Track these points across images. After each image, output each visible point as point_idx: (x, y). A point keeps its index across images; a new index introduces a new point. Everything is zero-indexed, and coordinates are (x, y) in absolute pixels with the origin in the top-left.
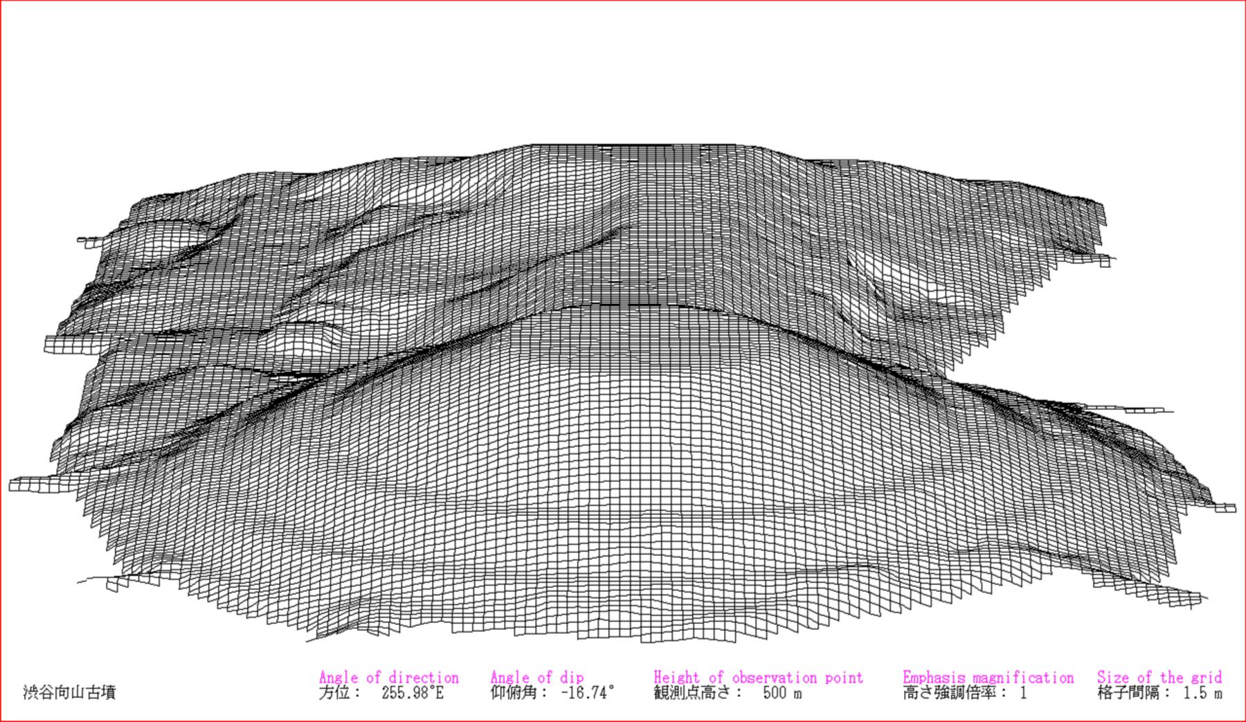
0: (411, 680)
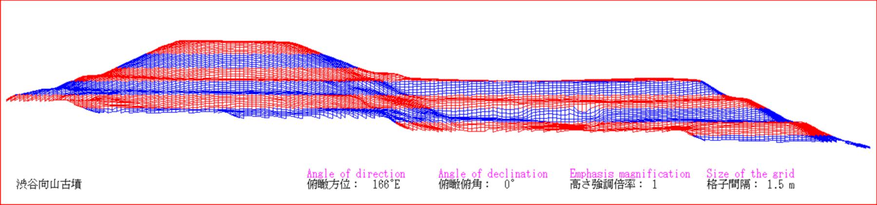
0: (371, 175)
